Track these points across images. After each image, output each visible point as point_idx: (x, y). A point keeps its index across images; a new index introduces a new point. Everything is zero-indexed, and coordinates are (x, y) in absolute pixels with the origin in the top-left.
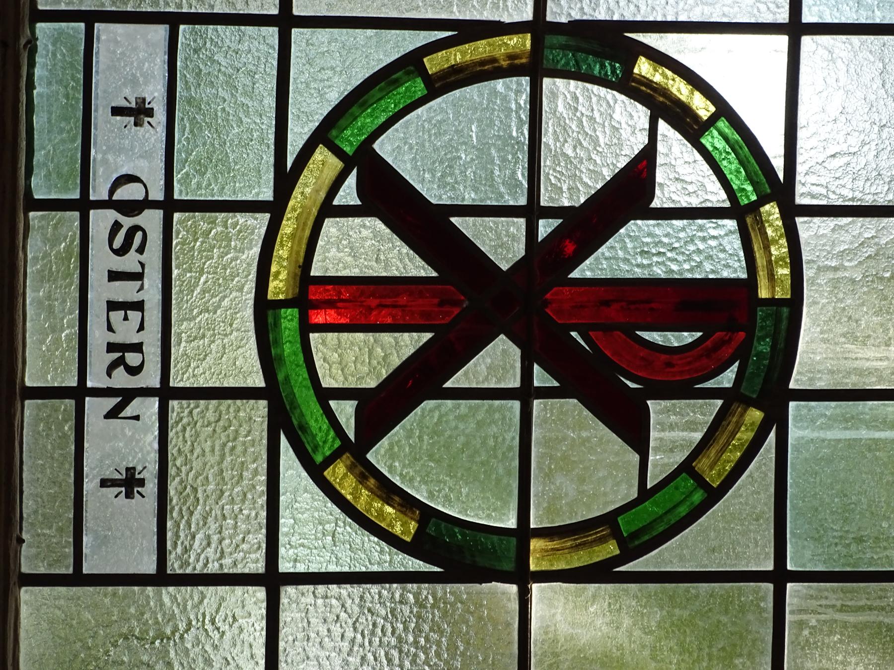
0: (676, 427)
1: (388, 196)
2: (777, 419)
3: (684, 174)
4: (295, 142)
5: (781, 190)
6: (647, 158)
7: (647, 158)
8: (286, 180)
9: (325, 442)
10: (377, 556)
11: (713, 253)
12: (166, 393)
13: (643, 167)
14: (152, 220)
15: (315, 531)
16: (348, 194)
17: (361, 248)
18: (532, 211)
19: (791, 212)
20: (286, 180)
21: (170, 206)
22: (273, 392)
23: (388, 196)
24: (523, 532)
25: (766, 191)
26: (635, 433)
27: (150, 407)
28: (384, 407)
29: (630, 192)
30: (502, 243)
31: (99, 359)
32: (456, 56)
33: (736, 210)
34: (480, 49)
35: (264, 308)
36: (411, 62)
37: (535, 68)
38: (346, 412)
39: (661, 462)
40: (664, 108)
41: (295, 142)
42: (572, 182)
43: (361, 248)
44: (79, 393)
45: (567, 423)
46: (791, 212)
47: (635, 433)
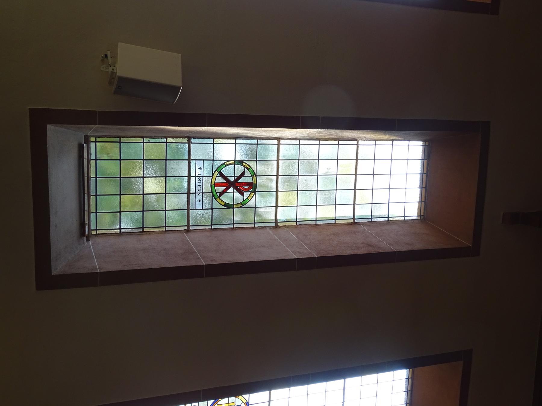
0: (246, 195)
1: (222, 175)
2: (255, 194)
3: (247, 173)
4: (214, 171)
5: (255, 174)
6: (244, 172)
7: (244, 172)
8: (213, 174)
9: (216, 197)
10: (245, 161)
11: (249, 180)
12: (195, 177)
13: (244, 172)
14: (201, 178)
15: (216, 205)
16: (219, 175)
17: (220, 180)
18: (234, 176)
19: (256, 176)
20: (213, 174)
21: (203, 177)
22: (212, 193)
23: (222, 175)
24: (234, 204)
25: (254, 174)
26: (243, 195)
27: (201, 194)
28: (222, 194)
29: (243, 175)
30: (232, 179)
31: (197, 190)
32: (228, 163)
33: (252, 176)
34: (230, 162)
35: (211, 185)
36: (224, 163)
37: (235, 164)
38: (218, 194)
39: (245, 198)
40: (246, 167)
41: (214, 171)
42: (237, 174)
43: (220, 180)
44: (195, 193)
45: (237, 195)
46: (256, 176)
47: (243, 195)
